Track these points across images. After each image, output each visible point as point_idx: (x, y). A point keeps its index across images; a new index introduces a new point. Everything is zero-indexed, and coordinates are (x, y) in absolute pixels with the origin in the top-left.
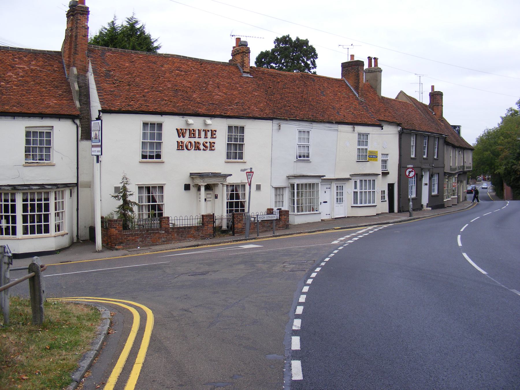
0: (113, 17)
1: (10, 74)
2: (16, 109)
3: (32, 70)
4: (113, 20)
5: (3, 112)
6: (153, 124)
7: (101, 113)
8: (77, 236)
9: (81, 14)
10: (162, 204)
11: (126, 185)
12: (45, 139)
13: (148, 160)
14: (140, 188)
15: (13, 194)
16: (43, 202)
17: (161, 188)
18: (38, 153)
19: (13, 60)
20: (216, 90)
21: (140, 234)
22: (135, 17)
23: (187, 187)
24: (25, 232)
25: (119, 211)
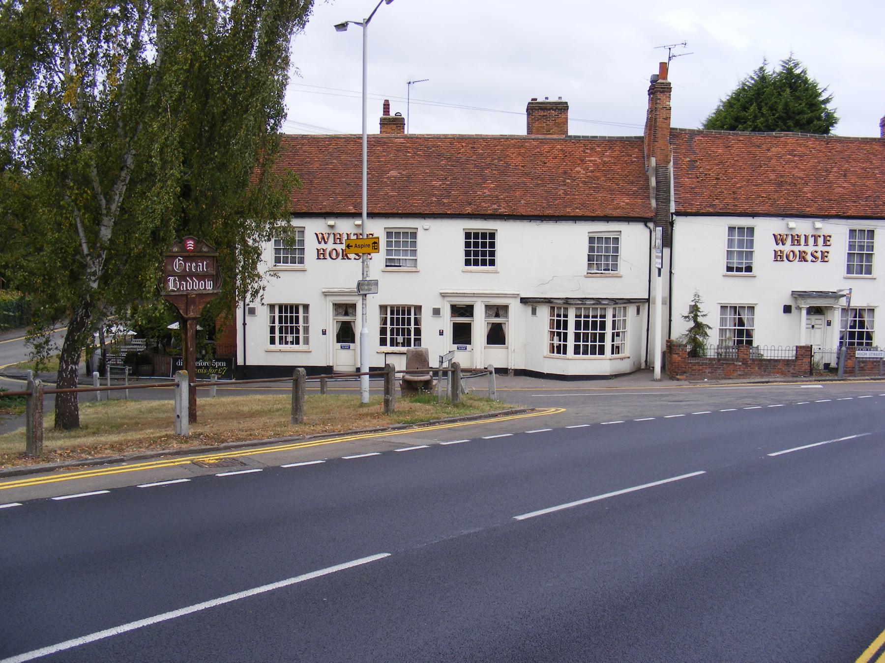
0: (762, 61)
1: (578, 169)
2: (578, 212)
3: (605, 163)
4: (763, 65)
5: (563, 216)
6: (741, 229)
7: (674, 216)
8: (646, 361)
9: (661, 92)
10: (752, 330)
11: (697, 304)
12: (611, 245)
13: (734, 273)
14: (724, 308)
15: (566, 309)
16: (599, 319)
17: (752, 308)
18: (603, 262)
19: (584, 152)
20: (842, 179)
21: (709, 364)
22: (793, 58)
23: (787, 309)
24: (577, 351)
25: (688, 334)
